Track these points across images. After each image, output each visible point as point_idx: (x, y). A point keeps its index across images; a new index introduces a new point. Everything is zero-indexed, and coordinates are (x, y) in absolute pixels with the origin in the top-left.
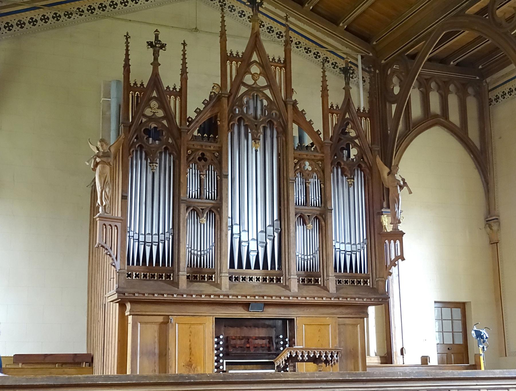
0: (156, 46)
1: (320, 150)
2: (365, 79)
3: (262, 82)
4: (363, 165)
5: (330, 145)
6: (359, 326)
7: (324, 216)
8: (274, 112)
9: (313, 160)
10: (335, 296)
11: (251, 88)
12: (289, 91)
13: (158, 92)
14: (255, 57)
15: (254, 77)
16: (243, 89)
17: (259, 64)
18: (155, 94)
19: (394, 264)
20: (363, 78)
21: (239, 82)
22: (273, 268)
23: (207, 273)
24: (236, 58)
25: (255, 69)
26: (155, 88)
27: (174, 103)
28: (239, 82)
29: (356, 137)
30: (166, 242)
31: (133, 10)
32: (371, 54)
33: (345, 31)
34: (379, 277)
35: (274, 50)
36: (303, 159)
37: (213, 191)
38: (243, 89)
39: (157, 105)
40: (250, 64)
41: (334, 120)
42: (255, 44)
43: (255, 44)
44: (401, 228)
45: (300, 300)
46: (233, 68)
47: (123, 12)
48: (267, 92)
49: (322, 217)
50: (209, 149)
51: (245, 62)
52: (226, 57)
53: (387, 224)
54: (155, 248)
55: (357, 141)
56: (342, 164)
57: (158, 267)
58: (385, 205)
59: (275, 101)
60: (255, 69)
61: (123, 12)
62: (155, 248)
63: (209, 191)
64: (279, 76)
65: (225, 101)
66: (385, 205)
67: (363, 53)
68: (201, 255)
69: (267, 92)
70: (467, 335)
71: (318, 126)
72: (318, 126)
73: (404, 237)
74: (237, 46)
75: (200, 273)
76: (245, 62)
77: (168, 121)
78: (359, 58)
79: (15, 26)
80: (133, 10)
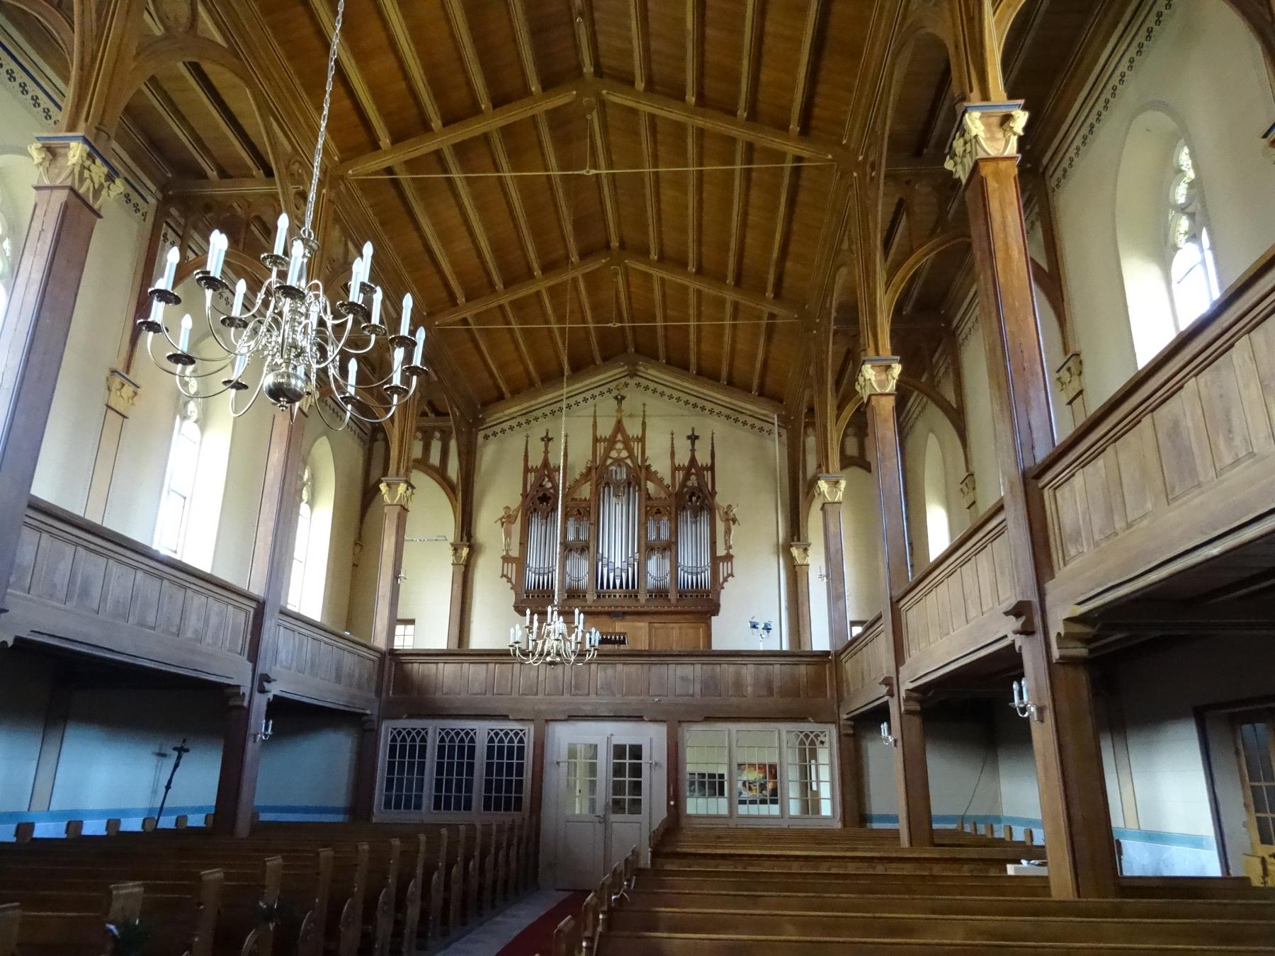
0: (547, 439)
3: (624, 454)
8: (549, 485)
12: (644, 459)
14: (619, 437)
15: (619, 452)
16: (609, 461)
19: (725, 580)
21: (607, 456)
24: (605, 440)
25: (619, 446)
28: (607, 456)
35: (633, 429)
38: (609, 461)
40: (615, 442)
42: (619, 427)
43: (619, 427)
44: (731, 552)
45: (646, 609)
46: (601, 447)
48: (628, 461)
51: (611, 442)
52: (596, 440)
60: (619, 446)
63: (665, 535)
64: (637, 448)
69: (628, 461)
70: (896, 651)
72: (667, 481)
73: (734, 560)
74: (606, 429)
76: (611, 442)
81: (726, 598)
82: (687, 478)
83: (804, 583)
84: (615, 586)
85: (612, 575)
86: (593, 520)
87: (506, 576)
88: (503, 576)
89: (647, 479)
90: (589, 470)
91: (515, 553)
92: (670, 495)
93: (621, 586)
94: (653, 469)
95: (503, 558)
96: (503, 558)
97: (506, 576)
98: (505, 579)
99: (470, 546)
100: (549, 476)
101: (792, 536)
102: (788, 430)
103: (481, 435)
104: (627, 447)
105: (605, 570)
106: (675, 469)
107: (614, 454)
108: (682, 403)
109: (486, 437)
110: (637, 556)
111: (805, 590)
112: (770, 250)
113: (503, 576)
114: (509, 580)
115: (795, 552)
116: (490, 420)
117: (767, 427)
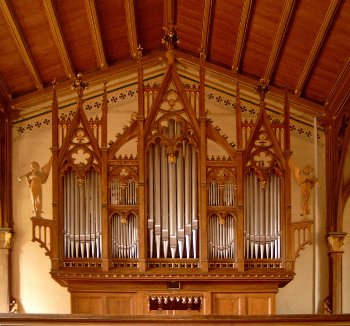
1: (234, 159)
2: (320, 136)
3: (179, 106)
4: (277, 169)
5: (242, 153)
6: (269, 299)
7: (236, 213)
9: (226, 167)
10: (243, 274)
11: (168, 114)
13: (84, 124)
14: (172, 86)
17: (176, 92)
18: (81, 126)
20: (318, 135)
21: (156, 109)
22: (191, 256)
23: (132, 262)
25: (172, 97)
26: (81, 121)
27: (97, 131)
28: (156, 109)
29: (271, 147)
30: (97, 240)
31: (121, 104)
32: (324, 115)
33: (301, 98)
34: (288, 259)
36: (217, 167)
37: (134, 198)
38: (159, 115)
39: (83, 134)
41: (248, 132)
47: (113, 107)
48: (184, 116)
49: (234, 213)
50: (128, 164)
53: (333, 244)
54: (87, 245)
55: (271, 150)
56: (256, 169)
57: (91, 258)
58: (332, 229)
59: (191, 122)
61: (113, 107)
62: (87, 245)
65: (141, 124)
66: (332, 229)
67: (317, 115)
68: (127, 249)
71: (232, 139)
75: (125, 261)
76: (163, 91)
77: (93, 147)
78: (315, 119)
79: (34, 126)
80: (121, 104)
81: (296, 271)
82: (255, 137)
83: (339, 267)
84: (169, 256)
85: (165, 244)
86: (142, 181)
87: (39, 241)
88: (34, 239)
89: (207, 137)
90: (135, 124)
91: (48, 214)
92: (235, 155)
93: (177, 256)
94: (214, 125)
95: (33, 219)
96: (33, 219)
97: (39, 241)
98: (37, 244)
99: (12, 232)
100: (85, 130)
101: (328, 229)
102: (326, 133)
103: (15, 131)
104: (182, 96)
105: (158, 238)
106: (241, 126)
107: (165, 106)
108: (222, 103)
109: (21, 130)
110: (195, 221)
111: (339, 273)
112: (125, 318)
113: (34, 239)
114: (43, 245)
115: (332, 240)
116: (26, 112)
117: (306, 129)
